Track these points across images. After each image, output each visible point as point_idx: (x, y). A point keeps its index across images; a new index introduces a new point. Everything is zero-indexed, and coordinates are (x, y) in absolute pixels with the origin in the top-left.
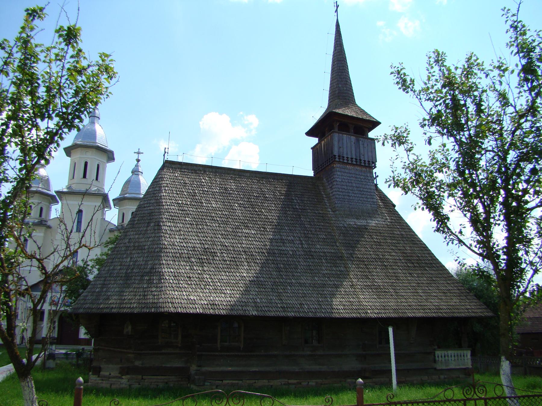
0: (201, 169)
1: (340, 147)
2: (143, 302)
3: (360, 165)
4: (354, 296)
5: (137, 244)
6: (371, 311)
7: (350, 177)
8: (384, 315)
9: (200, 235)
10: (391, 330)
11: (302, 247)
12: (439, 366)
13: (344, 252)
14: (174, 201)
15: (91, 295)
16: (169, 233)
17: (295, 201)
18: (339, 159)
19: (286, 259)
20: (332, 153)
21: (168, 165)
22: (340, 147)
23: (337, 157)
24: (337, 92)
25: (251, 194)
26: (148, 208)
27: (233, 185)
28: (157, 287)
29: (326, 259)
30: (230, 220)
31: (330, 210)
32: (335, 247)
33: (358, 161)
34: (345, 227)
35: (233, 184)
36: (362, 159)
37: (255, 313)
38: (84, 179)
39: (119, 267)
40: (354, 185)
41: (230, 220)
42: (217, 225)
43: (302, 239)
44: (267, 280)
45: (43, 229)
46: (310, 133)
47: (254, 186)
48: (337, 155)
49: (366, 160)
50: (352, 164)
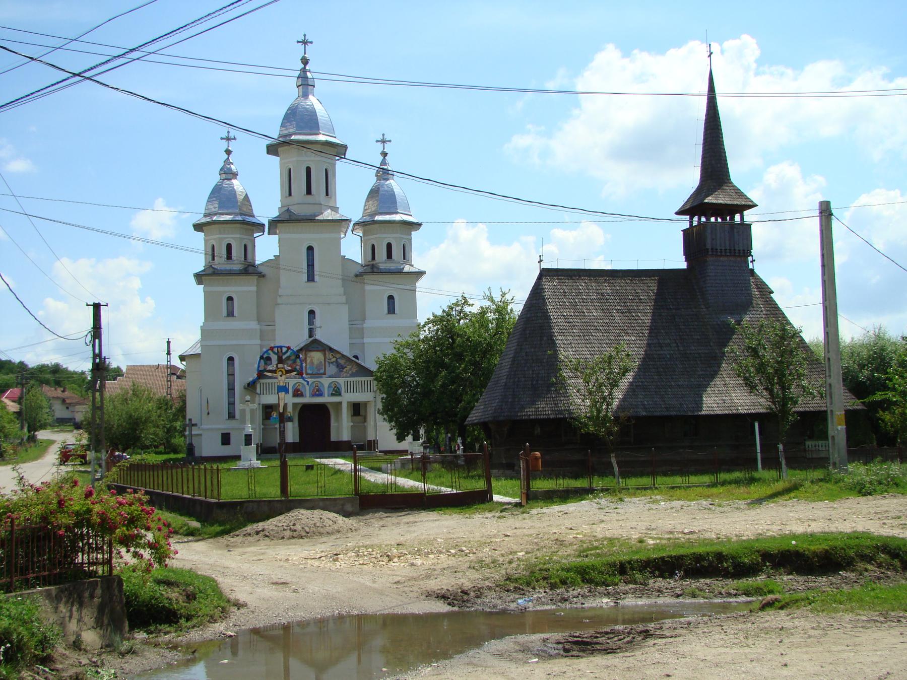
8: (753, 411)
10: (756, 425)
12: (809, 456)
20: (705, 245)
21: (545, 273)
27: (607, 289)
36: (737, 249)
37: (644, 414)
38: (309, 196)
45: (254, 278)
50: (726, 256)
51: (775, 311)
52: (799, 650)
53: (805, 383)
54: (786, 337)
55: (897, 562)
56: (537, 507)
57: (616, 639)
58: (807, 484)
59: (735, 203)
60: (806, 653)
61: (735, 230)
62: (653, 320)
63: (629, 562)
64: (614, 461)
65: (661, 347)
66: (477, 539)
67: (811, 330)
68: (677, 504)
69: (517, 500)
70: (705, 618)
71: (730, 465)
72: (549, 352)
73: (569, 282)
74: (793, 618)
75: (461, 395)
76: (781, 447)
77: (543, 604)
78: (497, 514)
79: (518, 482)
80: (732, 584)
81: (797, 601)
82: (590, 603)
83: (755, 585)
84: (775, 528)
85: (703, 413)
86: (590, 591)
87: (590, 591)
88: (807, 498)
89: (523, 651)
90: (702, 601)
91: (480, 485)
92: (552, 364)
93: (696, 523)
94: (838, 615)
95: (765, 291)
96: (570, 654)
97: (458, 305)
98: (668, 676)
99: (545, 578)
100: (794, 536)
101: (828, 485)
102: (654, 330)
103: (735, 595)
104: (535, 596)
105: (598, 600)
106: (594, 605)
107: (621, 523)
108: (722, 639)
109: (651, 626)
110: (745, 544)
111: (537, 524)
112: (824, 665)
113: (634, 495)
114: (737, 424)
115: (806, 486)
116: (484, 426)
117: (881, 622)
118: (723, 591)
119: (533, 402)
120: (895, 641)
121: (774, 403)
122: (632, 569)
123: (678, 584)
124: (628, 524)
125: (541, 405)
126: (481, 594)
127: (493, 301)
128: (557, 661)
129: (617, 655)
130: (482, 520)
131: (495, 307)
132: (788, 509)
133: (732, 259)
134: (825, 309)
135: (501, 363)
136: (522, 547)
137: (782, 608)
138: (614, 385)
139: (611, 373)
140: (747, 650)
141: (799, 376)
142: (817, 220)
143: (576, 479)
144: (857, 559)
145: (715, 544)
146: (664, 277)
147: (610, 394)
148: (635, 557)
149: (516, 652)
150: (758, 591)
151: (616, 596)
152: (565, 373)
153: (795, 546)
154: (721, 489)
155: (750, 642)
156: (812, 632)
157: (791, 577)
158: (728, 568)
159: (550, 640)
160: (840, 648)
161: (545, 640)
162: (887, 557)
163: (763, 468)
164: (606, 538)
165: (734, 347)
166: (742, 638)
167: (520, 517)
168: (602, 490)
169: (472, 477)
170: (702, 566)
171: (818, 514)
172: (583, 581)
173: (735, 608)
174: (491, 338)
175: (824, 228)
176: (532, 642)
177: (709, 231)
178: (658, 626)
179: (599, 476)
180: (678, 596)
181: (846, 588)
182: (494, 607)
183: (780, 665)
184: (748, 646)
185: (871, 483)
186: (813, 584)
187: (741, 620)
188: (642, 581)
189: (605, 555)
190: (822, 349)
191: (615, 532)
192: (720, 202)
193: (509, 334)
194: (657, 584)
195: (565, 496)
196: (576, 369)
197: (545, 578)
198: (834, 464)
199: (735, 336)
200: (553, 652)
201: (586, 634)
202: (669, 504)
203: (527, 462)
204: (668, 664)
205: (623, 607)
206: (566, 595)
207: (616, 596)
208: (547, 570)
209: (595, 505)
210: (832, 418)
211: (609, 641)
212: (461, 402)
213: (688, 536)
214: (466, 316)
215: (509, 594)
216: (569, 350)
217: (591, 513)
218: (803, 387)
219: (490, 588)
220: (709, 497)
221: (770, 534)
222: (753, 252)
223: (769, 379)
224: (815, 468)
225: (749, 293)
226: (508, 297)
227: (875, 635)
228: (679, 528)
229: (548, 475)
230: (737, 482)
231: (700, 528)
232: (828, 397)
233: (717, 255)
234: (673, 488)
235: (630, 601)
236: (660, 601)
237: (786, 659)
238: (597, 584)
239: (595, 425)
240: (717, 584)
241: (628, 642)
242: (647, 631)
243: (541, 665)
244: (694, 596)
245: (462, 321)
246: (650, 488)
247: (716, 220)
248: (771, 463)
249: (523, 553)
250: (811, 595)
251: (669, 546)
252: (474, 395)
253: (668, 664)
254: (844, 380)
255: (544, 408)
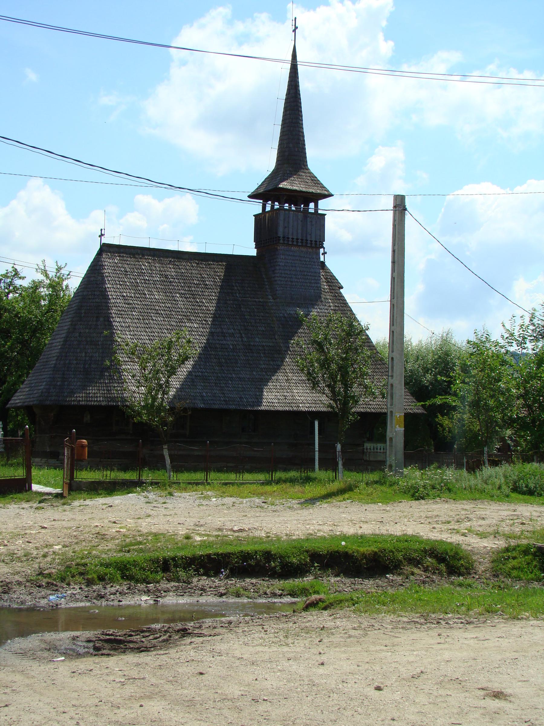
0: (139, 251)
1: (285, 227)
2: (109, 396)
3: (306, 246)
4: (289, 391)
5: (89, 339)
6: (303, 405)
7: (293, 260)
9: (147, 330)
10: (316, 423)
11: (242, 341)
13: (282, 345)
14: (119, 294)
15: (54, 388)
16: (120, 329)
17: (236, 288)
18: (284, 240)
19: (227, 354)
20: (277, 233)
21: (106, 249)
22: (285, 227)
23: (281, 238)
24: (287, 154)
25: (192, 282)
26: (94, 301)
27: (172, 272)
28: (119, 383)
29: (265, 353)
30: (174, 313)
31: (270, 297)
32: (274, 340)
33: (304, 241)
34: (285, 317)
35: (173, 270)
36: (309, 239)
37: (202, 406)
39: (75, 362)
40: (298, 269)
41: (174, 313)
42: (162, 319)
43: (241, 332)
44: (211, 374)
46: (254, 196)
47: (193, 272)
48: (282, 236)
49: (313, 239)
51: (343, 306)
52: (337, 649)
53: (367, 382)
54: (353, 332)
55: (443, 567)
56: (80, 499)
57: (151, 637)
58: (362, 485)
59: (311, 190)
60: (345, 652)
61: (309, 219)
62: (218, 307)
63: (173, 559)
64: (166, 453)
65: (224, 336)
66: (9, 531)
67: (379, 333)
68: (228, 500)
69: (59, 491)
70: (247, 618)
71: (286, 464)
72: (105, 332)
73: (131, 261)
74: (335, 618)
75: (5, 376)
76: (339, 447)
77: (77, 600)
78: (35, 505)
79: (62, 472)
80: (278, 584)
81: (341, 601)
82: (128, 601)
83: (301, 585)
84: (326, 528)
85: (263, 408)
86: (129, 588)
87: (129, 588)
88: (360, 500)
89: (49, 650)
90: (246, 600)
91: (19, 473)
92: (108, 346)
93: (246, 520)
94: (380, 616)
95: (335, 286)
96: (100, 652)
97: (8, 277)
98: (201, 674)
99: (81, 574)
100: (344, 537)
101: (383, 488)
102: (217, 317)
103: (280, 596)
104: (69, 592)
105: (137, 598)
106: (132, 602)
107: (168, 518)
108: (262, 638)
109: (190, 625)
110: (296, 544)
111: (78, 517)
112: (360, 664)
113: (185, 489)
114: (296, 421)
115: (361, 488)
116: (29, 410)
117: (421, 624)
118: (268, 591)
119: (84, 387)
120: (433, 642)
121: (335, 401)
122: (176, 566)
123: (222, 583)
124: (176, 520)
125: (92, 390)
126: (9, 589)
127: (47, 276)
128: (85, 659)
129: (150, 653)
130: (17, 511)
131: (48, 282)
132: (341, 510)
133: (304, 249)
134: (392, 306)
135: (51, 343)
136: (59, 540)
137: (325, 609)
138: (172, 372)
139: (170, 359)
140: (286, 649)
141: (363, 375)
142: (391, 213)
143: (125, 471)
144: (405, 563)
145: (263, 542)
146: (232, 262)
147: (167, 382)
148: (181, 554)
149: (42, 650)
150: (304, 592)
151: (157, 594)
152: (121, 357)
153: (345, 547)
154: (275, 488)
155: (290, 641)
156: (352, 632)
157: (339, 579)
158: (275, 567)
159: (81, 639)
160: (378, 648)
161: (74, 638)
162: (434, 561)
163: (320, 469)
164: (150, 533)
165: (300, 341)
166: (281, 637)
167: (60, 509)
168: (152, 484)
169: (11, 465)
170: (250, 565)
171: (370, 516)
172: (122, 578)
173: (280, 609)
174: (43, 316)
175: (397, 219)
176: (60, 640)
177: (282, 218)
178: (198, 625)
179: (150, 469)
180: (221, 595)
181: (390, 591)
182: (22, 603)
183: (317, 664)
184: (287, 645)
185: (424, 487)
186: (360, 587)
187: (284, 619)
188: (185, 578)
189: (149, 550)
190: (387, 350)
191: (161, 527)
192: (295, 188)
193: (62, 312)
194: (201, 583)
195: (111, 488)
196: (133, 354)
197: (81, 574)
198: (391, 466)
199: (301, 330)
200: (82, 651)
201: (119, 633)
202: (220, 501)
203: (72, 450)
204: (202, 662)
205: (163, 606)
206: (103, 592)
207: (157, 594)
208: (85, 565)
209: (143, 499)
210: (391, 419)
211: (143, 640)
212: (4, 383)
213: (237, 534)
214: (15, 290)
215: (41, 589)
216: (127, 332)
217: (137, 507)
218: (366, 387)
219: (19, 583)
220: (262, 494)
221: (320, 534)
222: (325, 244)
223: (333, 377)
224: (372, 471)
225: (319, 286)
226: (64, 271)
227: (414, 636)
228: (229, 525)
229: (94, 466)
230: (292, 481)
231: (250, 526)
232: (389, 397)
233: (288, 245)
234: (226, 484)
235: (170, 600)
236: (203, 600)
237: (323, 658)
238: (137, 581)
239: (148, 414)
240: (262, 584)
241: (164, 641)
242: (185, 630)
243: (67, 663)
244: (238, 595)
245: (11, 295)
246: (202, 484)
247: (290, 206)
248: (329, 464)
249: (60, 547)
250: (355, 596)
251: (216, 544)
252: (20, 376)
253: (202, 662)
254: (406, 384)
255: (95, 394)
